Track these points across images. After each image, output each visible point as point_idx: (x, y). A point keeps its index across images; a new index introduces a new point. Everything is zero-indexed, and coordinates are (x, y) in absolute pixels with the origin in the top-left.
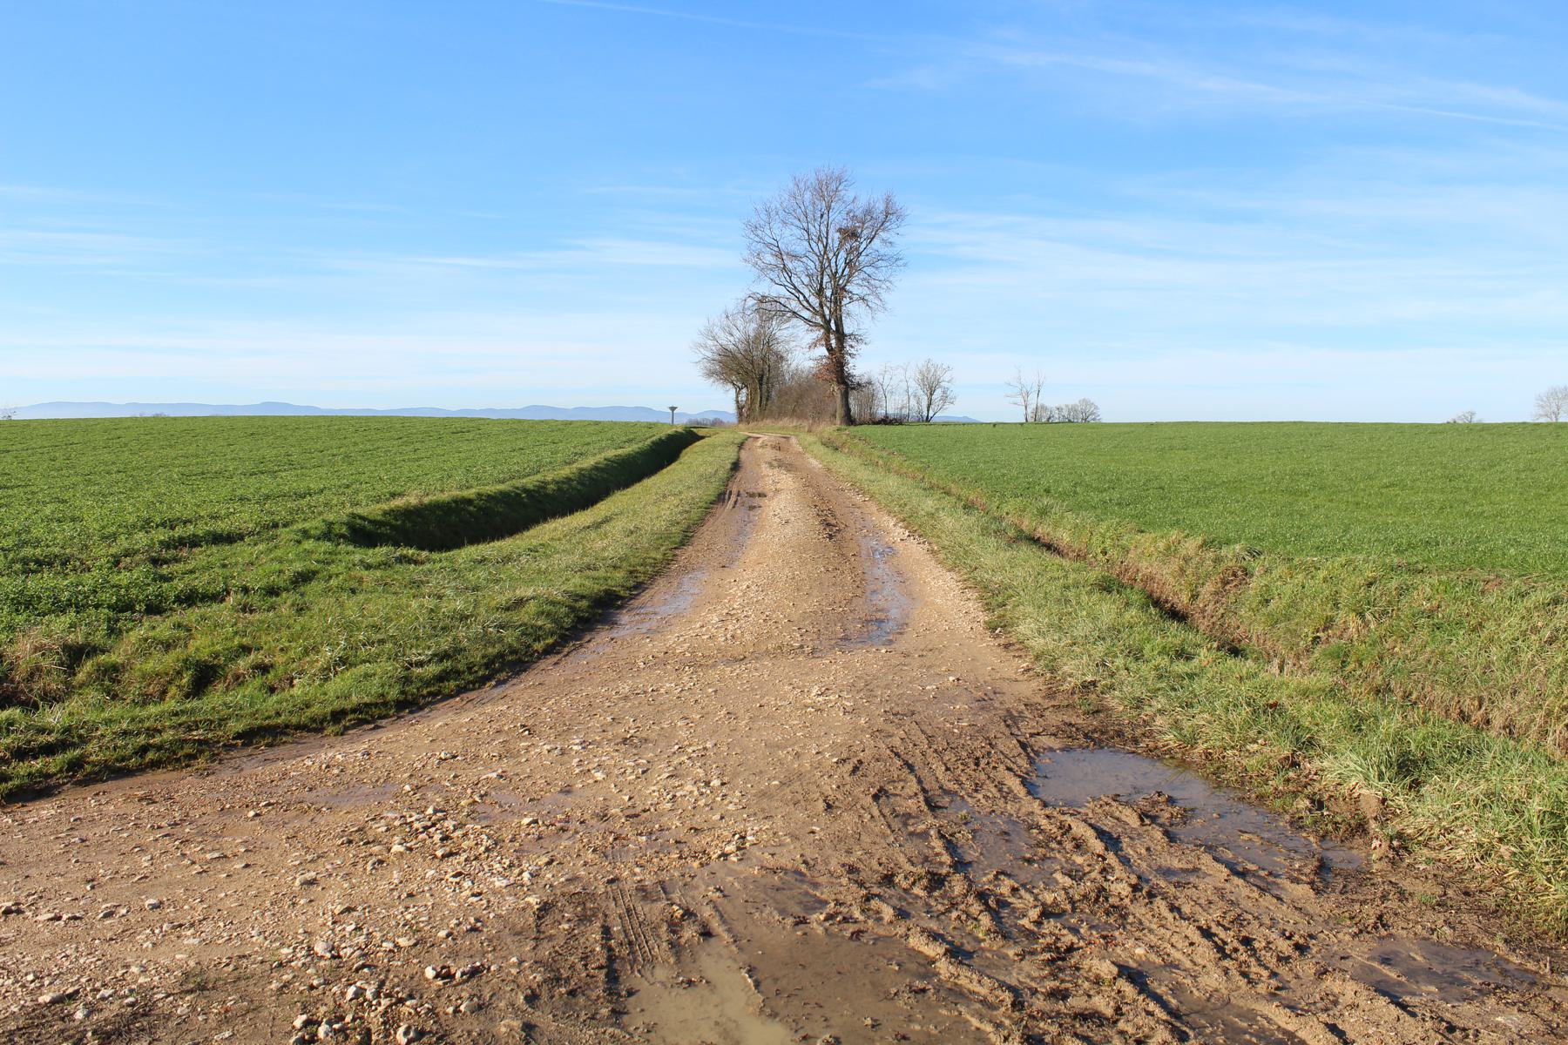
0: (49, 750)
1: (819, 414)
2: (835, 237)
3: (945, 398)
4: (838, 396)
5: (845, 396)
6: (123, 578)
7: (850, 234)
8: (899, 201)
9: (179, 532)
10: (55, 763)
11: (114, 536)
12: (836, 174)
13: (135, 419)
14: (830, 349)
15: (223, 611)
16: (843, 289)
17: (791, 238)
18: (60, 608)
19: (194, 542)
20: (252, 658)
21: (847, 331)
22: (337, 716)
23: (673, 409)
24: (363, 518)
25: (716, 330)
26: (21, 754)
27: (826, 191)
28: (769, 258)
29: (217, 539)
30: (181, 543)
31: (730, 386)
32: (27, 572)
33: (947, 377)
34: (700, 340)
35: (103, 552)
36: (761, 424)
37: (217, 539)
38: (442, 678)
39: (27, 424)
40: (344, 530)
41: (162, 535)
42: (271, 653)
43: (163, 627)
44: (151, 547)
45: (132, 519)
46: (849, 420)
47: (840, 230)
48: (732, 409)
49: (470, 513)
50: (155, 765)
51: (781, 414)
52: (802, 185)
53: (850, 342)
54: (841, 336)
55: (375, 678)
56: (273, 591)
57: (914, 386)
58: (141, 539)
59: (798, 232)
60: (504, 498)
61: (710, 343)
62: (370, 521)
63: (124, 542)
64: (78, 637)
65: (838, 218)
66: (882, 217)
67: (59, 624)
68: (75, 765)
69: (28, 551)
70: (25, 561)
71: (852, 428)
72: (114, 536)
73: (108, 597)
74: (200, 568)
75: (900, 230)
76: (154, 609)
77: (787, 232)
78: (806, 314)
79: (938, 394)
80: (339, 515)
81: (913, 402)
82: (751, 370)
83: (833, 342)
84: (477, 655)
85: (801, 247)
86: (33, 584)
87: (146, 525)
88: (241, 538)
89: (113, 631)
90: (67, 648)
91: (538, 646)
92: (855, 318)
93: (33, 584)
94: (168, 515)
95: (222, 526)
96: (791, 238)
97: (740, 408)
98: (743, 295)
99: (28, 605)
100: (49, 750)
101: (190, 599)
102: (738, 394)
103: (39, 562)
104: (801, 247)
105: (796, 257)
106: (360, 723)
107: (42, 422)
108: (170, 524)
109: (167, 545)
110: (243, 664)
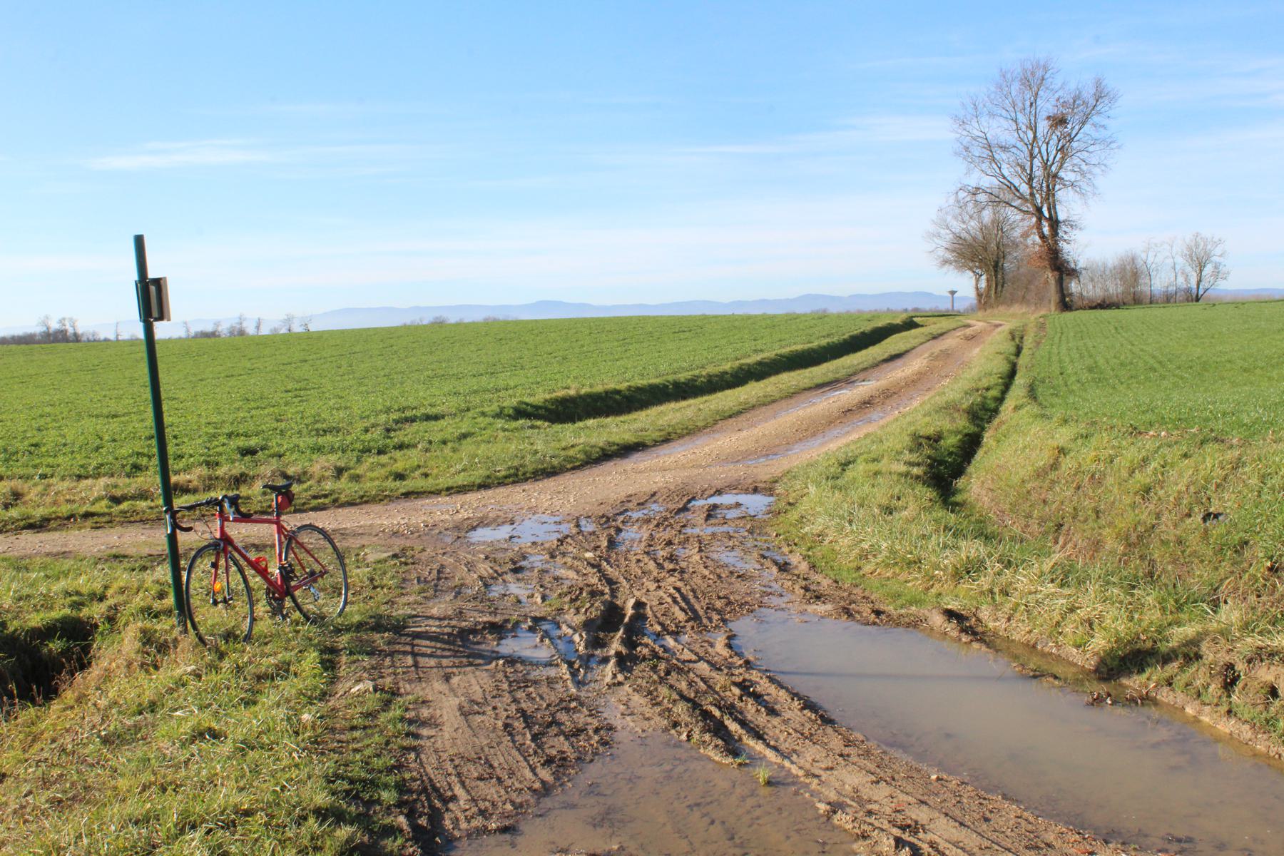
0: (325, 496)
1: (1040, 300)
2: (1043, 126)
3: (1217, 273)
4: (1052, 282)
5: (1060, 282)
6: (368, 436)
7: (1059, 121)
8: (1110, 83)
9: (408, 414)
10: (327, 501)
11: (368, 417)
12: (1042, 63)
13: (405, 327)
14: (1042, 237)
15: (413, 453)
16: (1055, 176)
17: (1000, 130)
18: (333, 450)
19: (413, 420)
20: (422, 471)
21: (1061, 217)
22: (448, 489)
23: (953, 293)
24: (527, 404)
25: (949, 218)
26: (315, 497)
27: (1034, 80)
28: (977, 151)
29: (428, 418)
30: (407, 420)
31: (970, 274)
32: (318, 435)
33: (1218, 251)
34: (932, 228)
35: (360, 426)
36: (996, 311)
37: (428, 418)
38: (506, 477)
39: (320, 336)
40: (511, 411)
41: (395, 416)
42: (432, 468)
43: (384, 459)
44: (387, 422)
45: (380, 407)
46: (1066, 305)
47: (1049, 118)
48: (972, 294)
49: (615, 401)
50: (366, 502)
51: (1012, 301)
52: (1009, 76)
53: (1064, 228)
54: (1055, 223)
55: (478, 475)
56: (444, 442)
57: (1180, 261)
58: (383, 418)
59: (1005, 124)
60: (639, 390)
61: (943, 232)
62: (532, 406)
63: (372, 420)
64: (341, 464)
65: (1047, 106)
66: (1092, 102)
67: (333, 458)
68: (335, 501)
69: (318, 426)
70: (317, 430)
71: (1068, 315)
72: (368, 417)
73: (358, 446)
74: (406, 434)
75: (1111, 113)
76: (380, 452)
77: (994, 123)
78: (1017, 203)
79: (1208, 269)
80: (510, 402)
81: (1181, 280)
82: (983, 254)
83: (1046, 230)
84: (530, 468)
85: (1009, 137)
86: (321, 440)
87: (388, 411)
88: (443, 417)
89: (359, 460)
90: (336, 467)
91: (569, 466)
92: (1068, 205)
93: (321, 440)
94: (405, 404)
95: (434, 411)
96: (1000, 130)
97: (979, 295)
98: (954, 189)
99: (319, 450)
100: (325, 496)
101: (401, 447)
102: (977, 281)
103: (325, 431)
104: (1009, 137)
105: (1004, 148)
106: (459, 492)
107: (331, 333)
108: (403, 410)
109: (397, 422)
110: (417, 473)
